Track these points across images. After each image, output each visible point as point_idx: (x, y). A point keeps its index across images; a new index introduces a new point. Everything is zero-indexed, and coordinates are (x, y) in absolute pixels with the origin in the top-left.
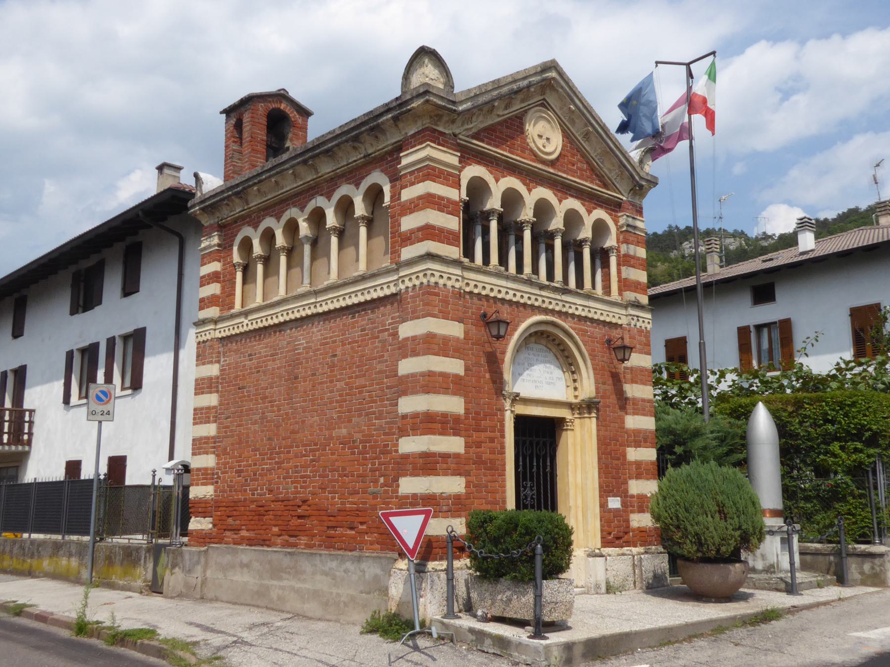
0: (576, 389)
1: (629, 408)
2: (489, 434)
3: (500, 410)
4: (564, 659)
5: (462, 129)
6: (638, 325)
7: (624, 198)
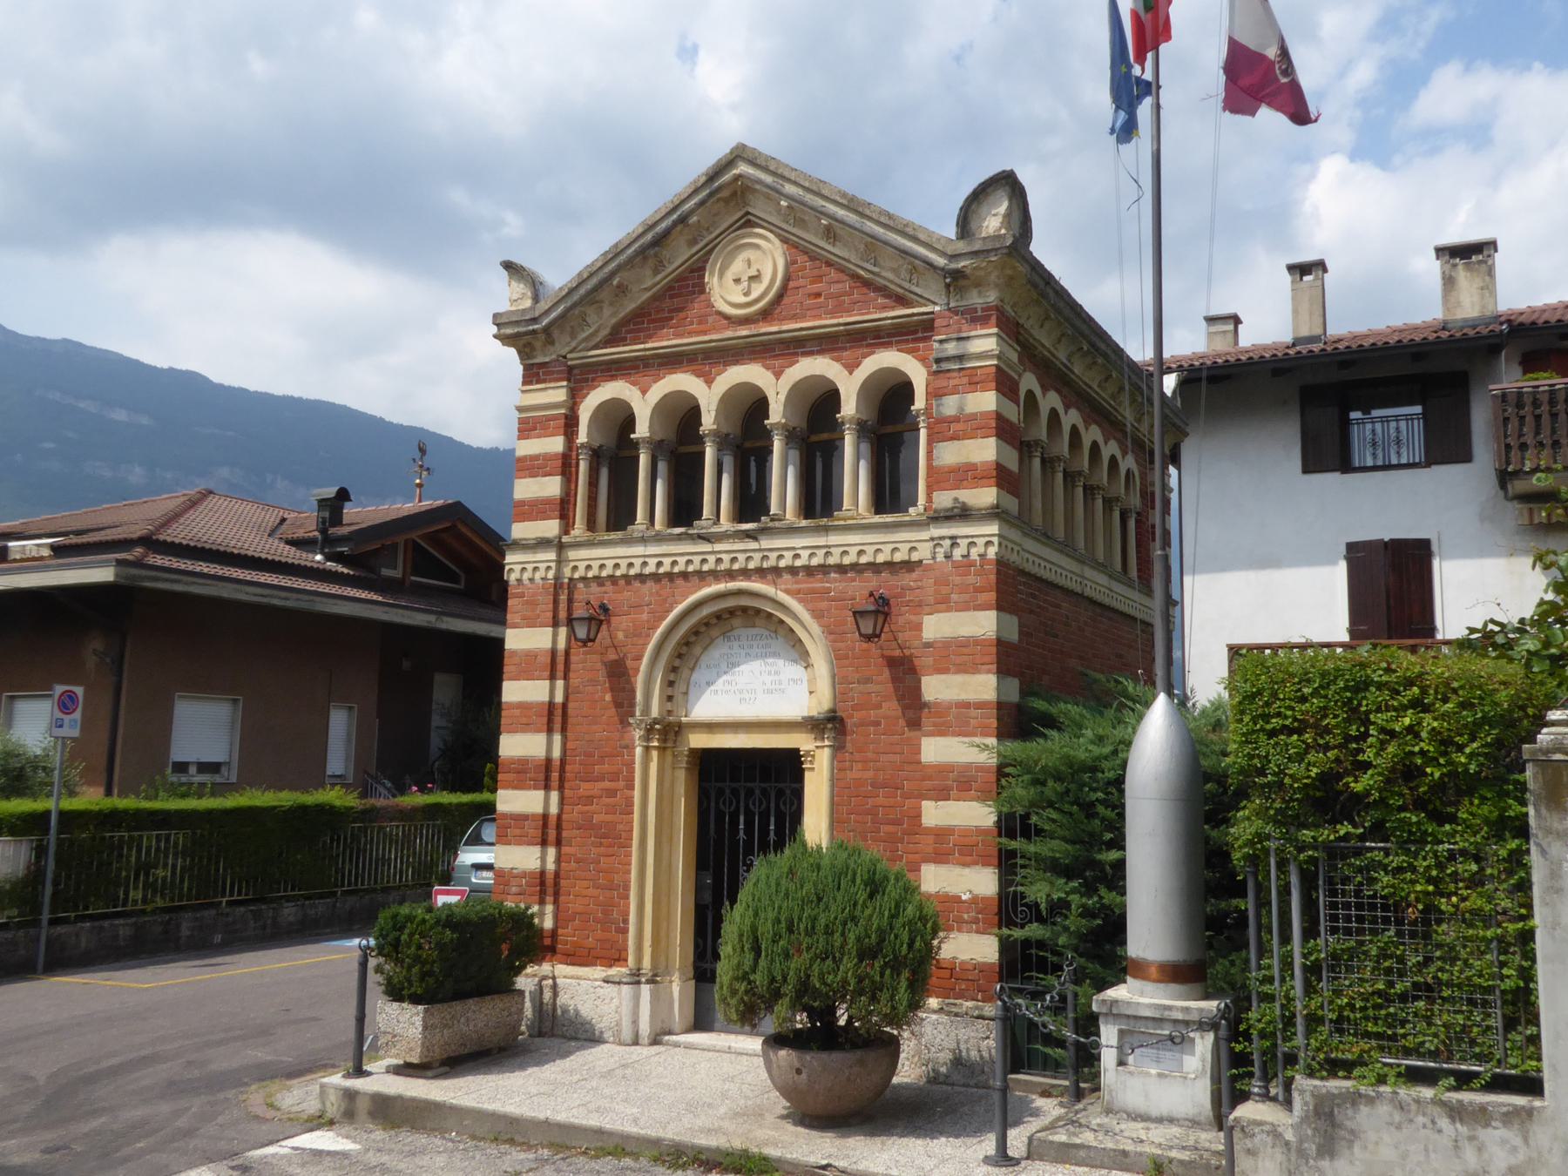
1: (927, 722)
2: (607, 784)
3: (626, 747)
6: (957, 554)
7: (937, 308)
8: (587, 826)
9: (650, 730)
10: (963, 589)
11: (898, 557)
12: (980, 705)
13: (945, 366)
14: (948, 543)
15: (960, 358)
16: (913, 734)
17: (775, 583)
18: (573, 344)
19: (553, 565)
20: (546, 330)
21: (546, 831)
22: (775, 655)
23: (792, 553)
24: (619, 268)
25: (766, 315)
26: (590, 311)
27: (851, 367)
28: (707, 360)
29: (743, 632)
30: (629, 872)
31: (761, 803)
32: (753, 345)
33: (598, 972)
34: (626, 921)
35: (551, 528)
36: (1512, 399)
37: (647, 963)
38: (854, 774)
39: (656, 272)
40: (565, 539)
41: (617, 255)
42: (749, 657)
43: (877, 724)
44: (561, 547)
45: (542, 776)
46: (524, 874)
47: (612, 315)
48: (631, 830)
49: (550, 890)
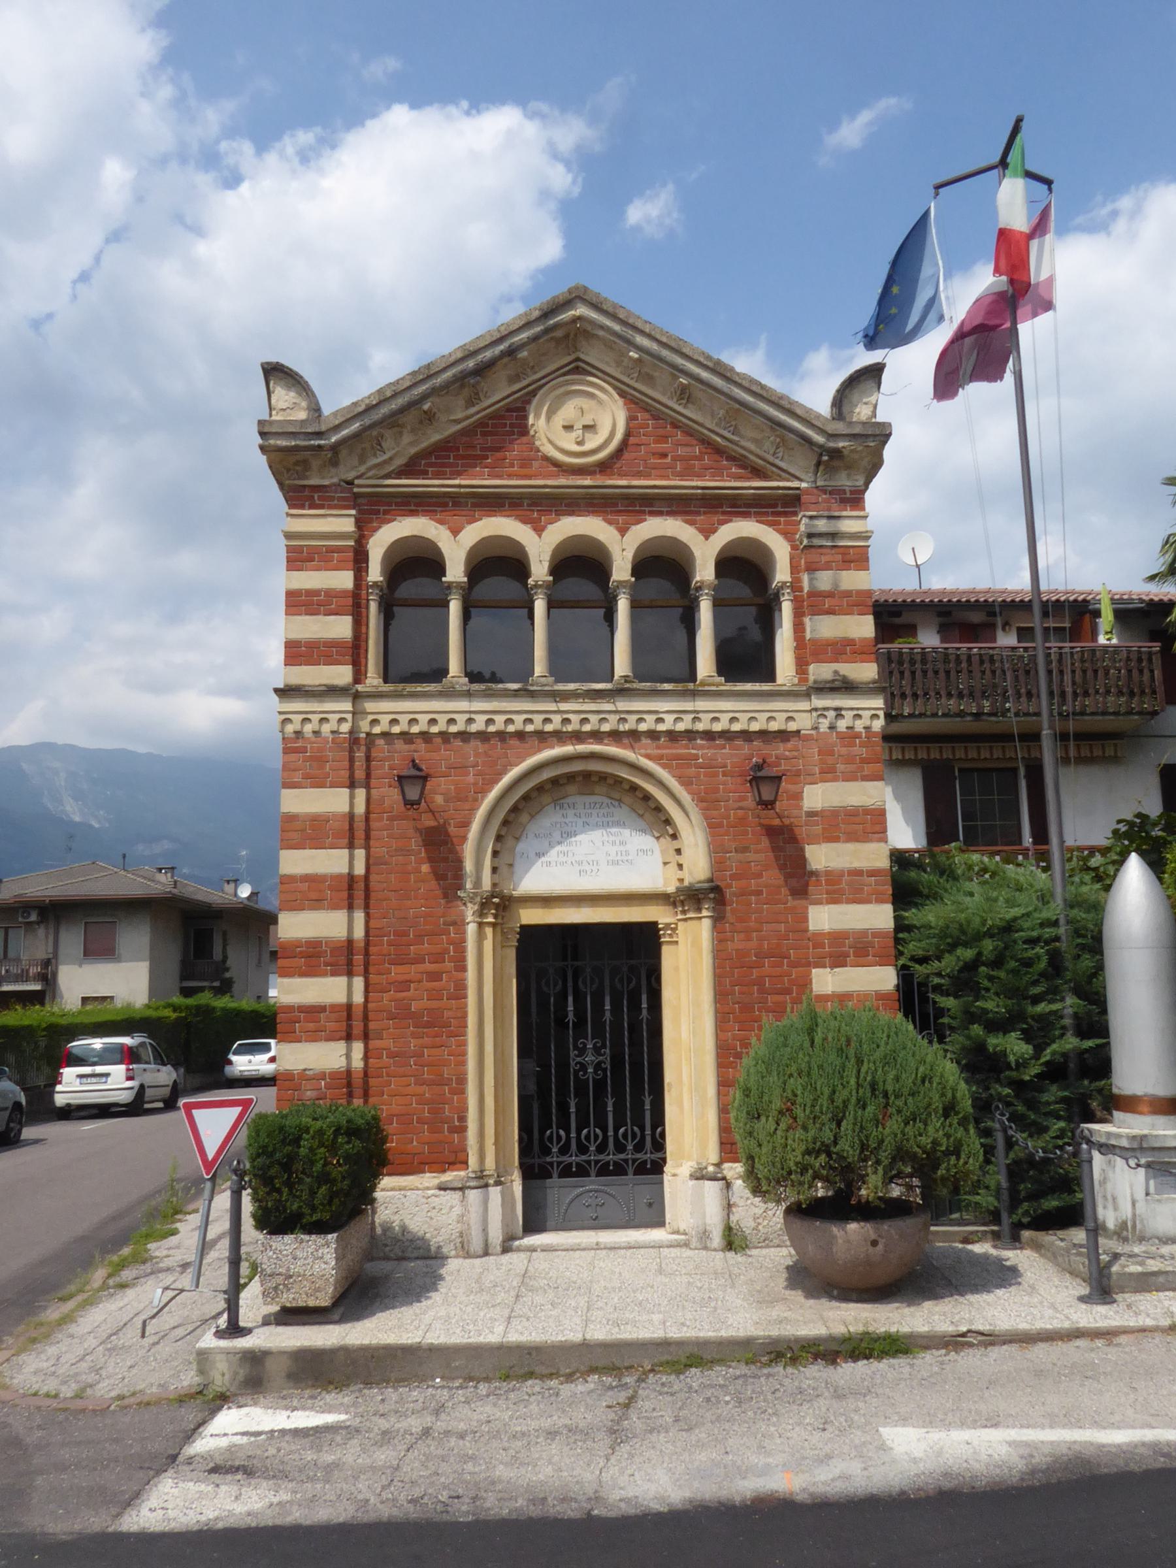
0: (680, 866)
3: (454, 923)
4: (241, 1377)
5: (362, 469)
6: (842, 725)
7: (804, 485)
8: (403, 1014)
9: (484, 906)
10: (849, 760)
11: (774, 726)
12: (873, 873)
13: (817, 542)
14: (832, 714)
15: (833, 535)
16: (796, 903)
17: (632, 748)
18: (362, 469)
19: (349, 717)
20: (335, 448)
21: (347, 1023)
22: (618, 824)
23: (655, 717)
24: (434, 391)
25: (604, 467)
26: (388, 433)
27: (707, 532)
28: (538, 507)
29: (580, 799)
30: (464, 1063)
31: (629, 981)
32: (592, 497)
33: (429, 1179)
34: (463, 1119)
35: (342, 674)
36: (895, 657)
37: (490, 1163)
38: (736, 944)
39: (470, 403)
40: (360, 687)
41: (429, 377)
42: (587, 826)
43: (759, 893)
44: (357, 697)
45: (343, 960)
46: (322, 1076)
47: (411, 444)
48: (464, 1016)
49: (358, 1091)
